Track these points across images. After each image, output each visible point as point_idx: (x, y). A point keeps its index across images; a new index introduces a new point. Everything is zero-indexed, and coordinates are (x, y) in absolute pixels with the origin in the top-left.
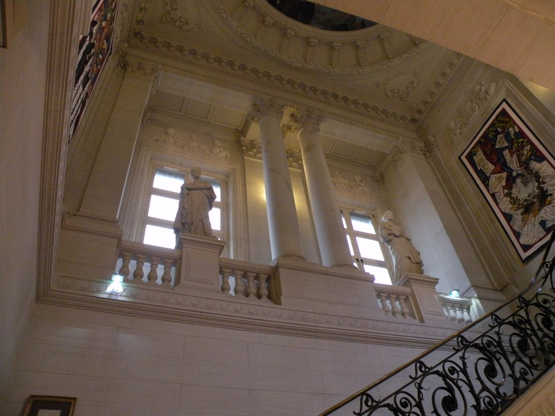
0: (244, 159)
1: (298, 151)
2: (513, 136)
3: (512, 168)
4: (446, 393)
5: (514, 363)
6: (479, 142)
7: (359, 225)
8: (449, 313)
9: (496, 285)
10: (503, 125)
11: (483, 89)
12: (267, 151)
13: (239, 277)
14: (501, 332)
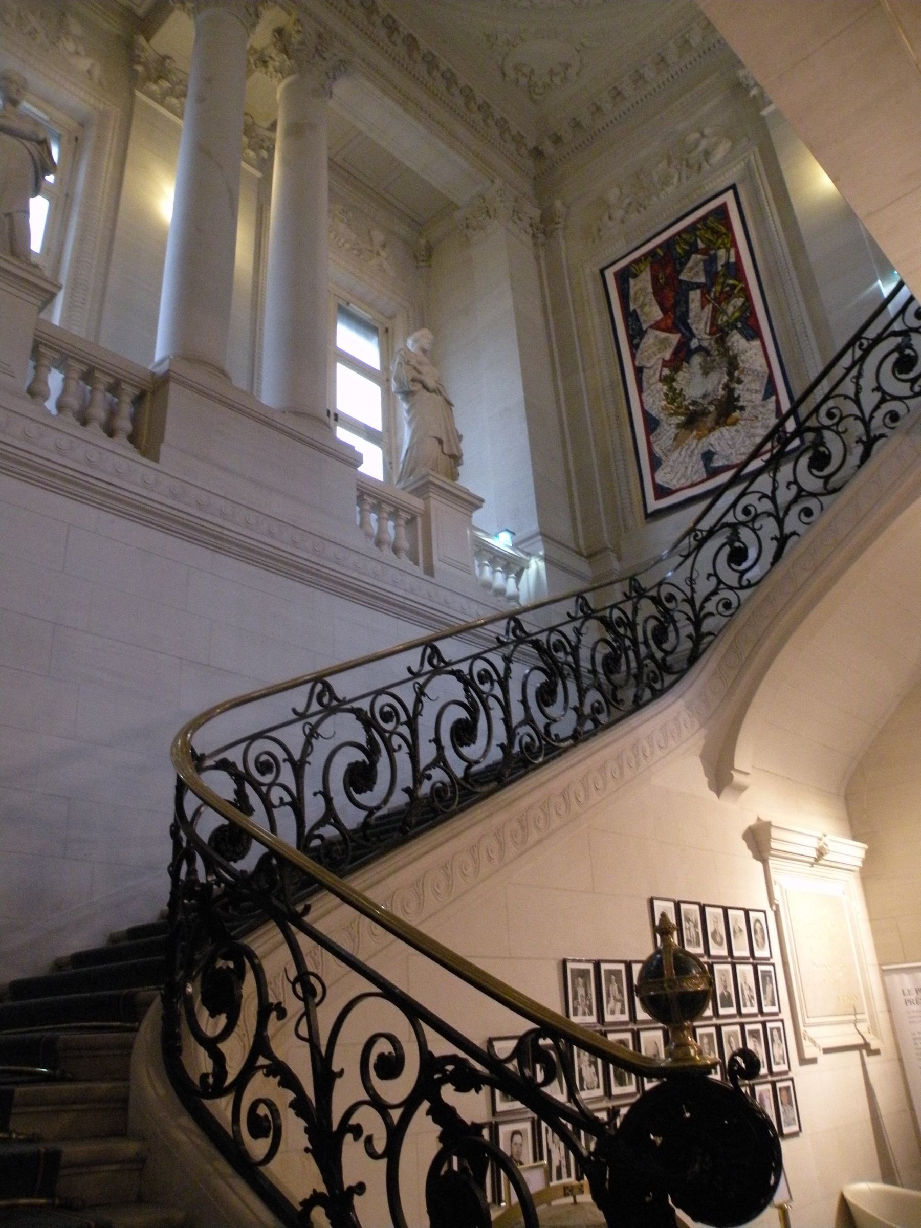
0: (132, 95)
1: (266, 124)
2: (720, 268)
3: (695, 331)
4: (463, 714)
5: (588, 689)
6: (652, 253)
7: (349, 339)
8: (482, 572)
9: (582, 543)
10: (712, 238)
11: (704, 144)
12: (200, 99)
13: (75, 375)
14: (584, 631)
